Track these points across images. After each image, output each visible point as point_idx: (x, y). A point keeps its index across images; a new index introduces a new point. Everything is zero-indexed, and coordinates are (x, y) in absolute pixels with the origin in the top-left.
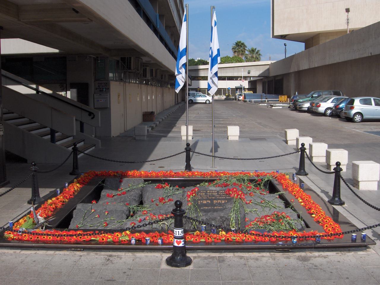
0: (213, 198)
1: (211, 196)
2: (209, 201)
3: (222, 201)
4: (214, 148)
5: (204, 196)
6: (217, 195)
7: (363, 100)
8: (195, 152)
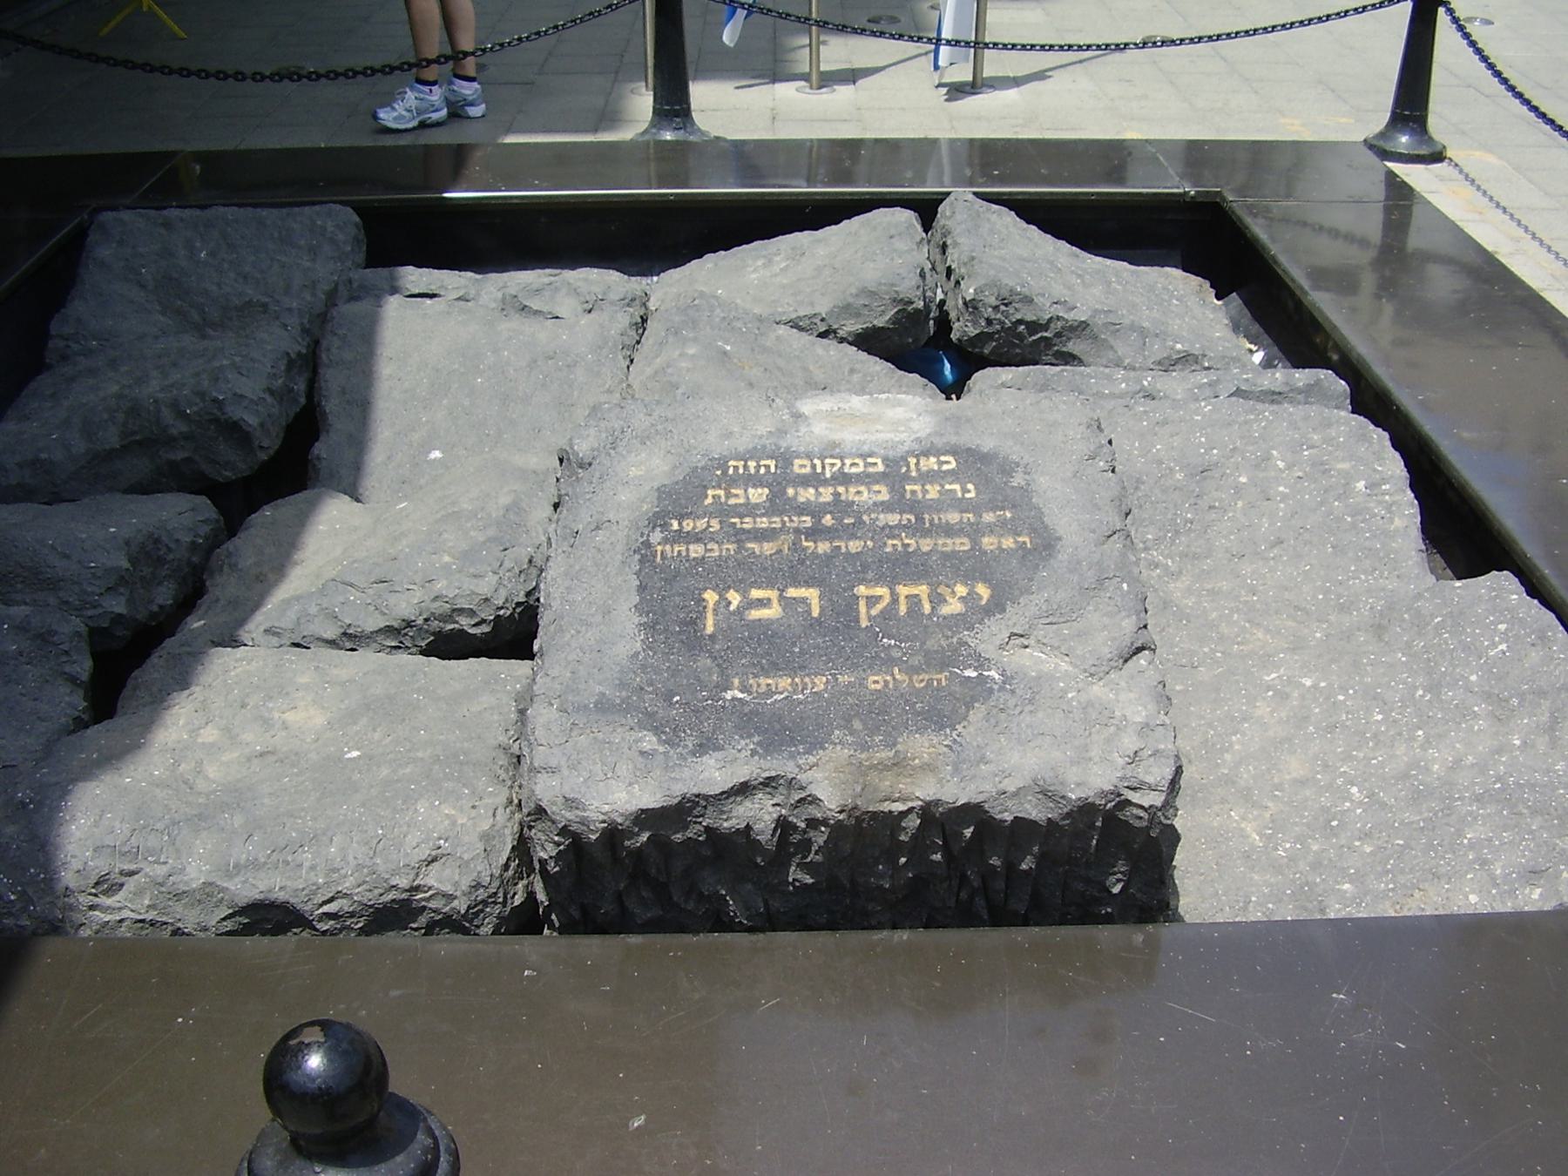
0: (855, 546)
1: (828, 520)
2: (812, 594)
3: (928, 487)
4: (1002, 181)
5: (763, 523)
6: (887, 507)
7: (904, 26)
8: (986, 45)
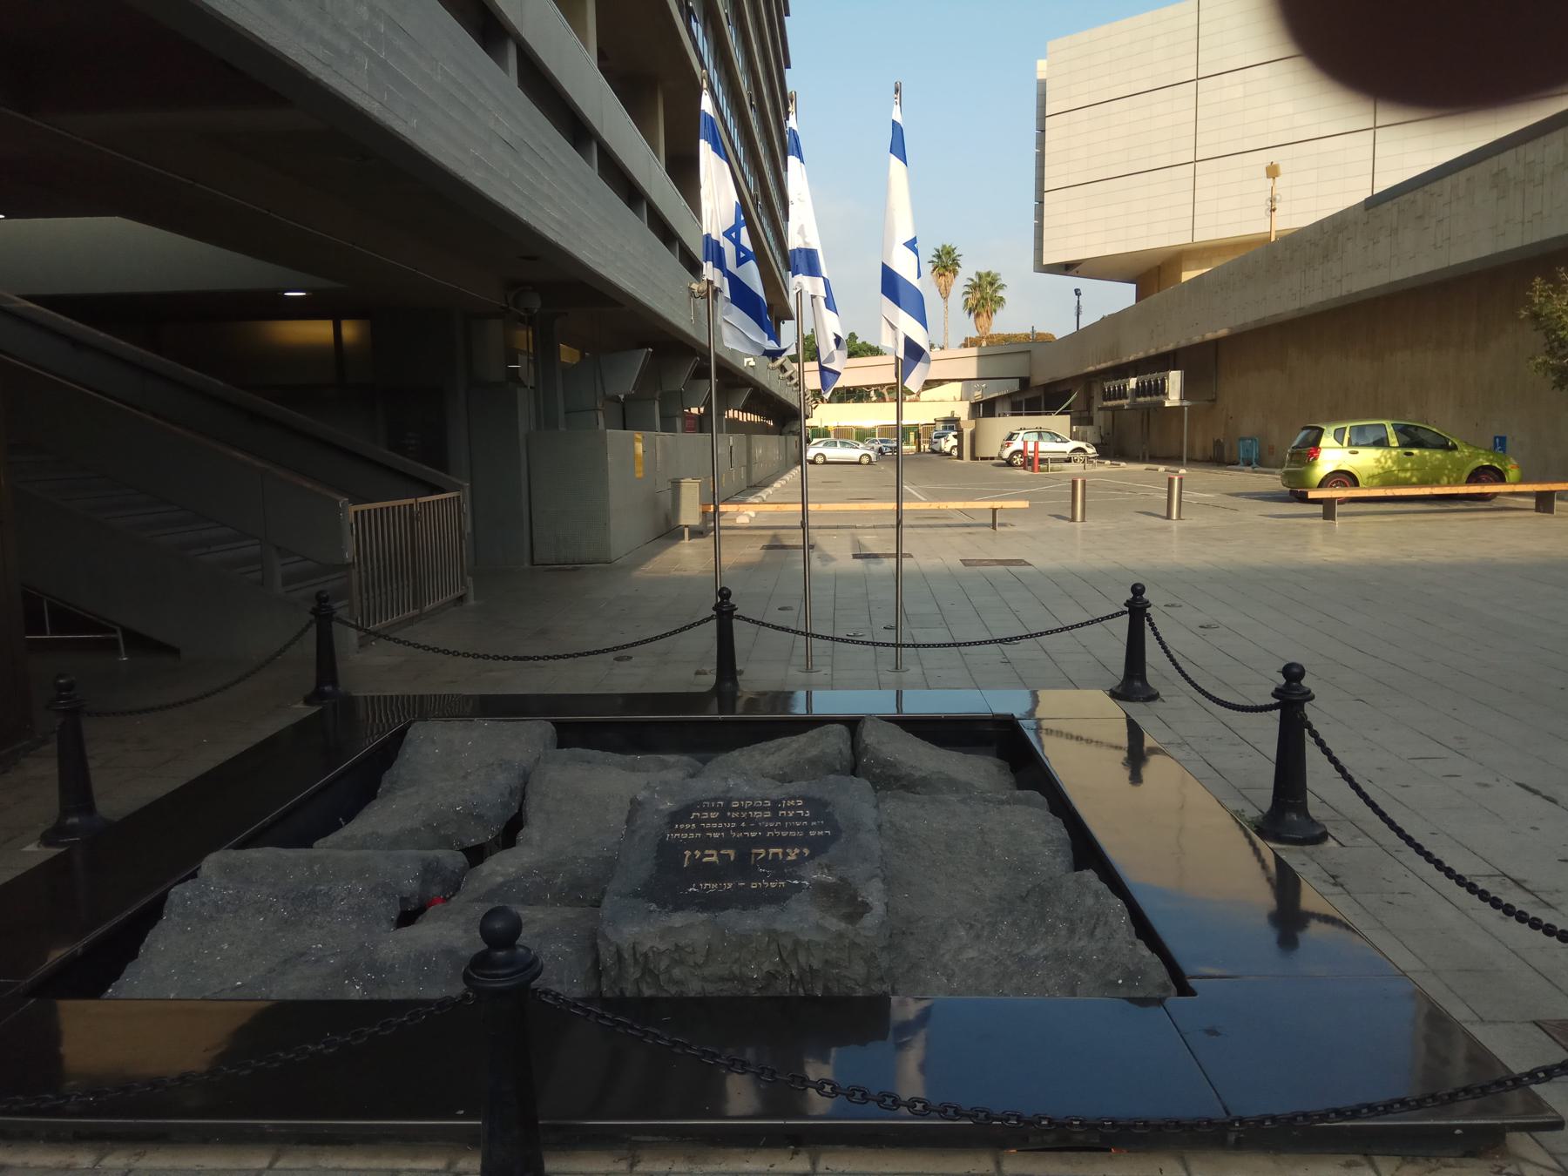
6: (769, 820)
